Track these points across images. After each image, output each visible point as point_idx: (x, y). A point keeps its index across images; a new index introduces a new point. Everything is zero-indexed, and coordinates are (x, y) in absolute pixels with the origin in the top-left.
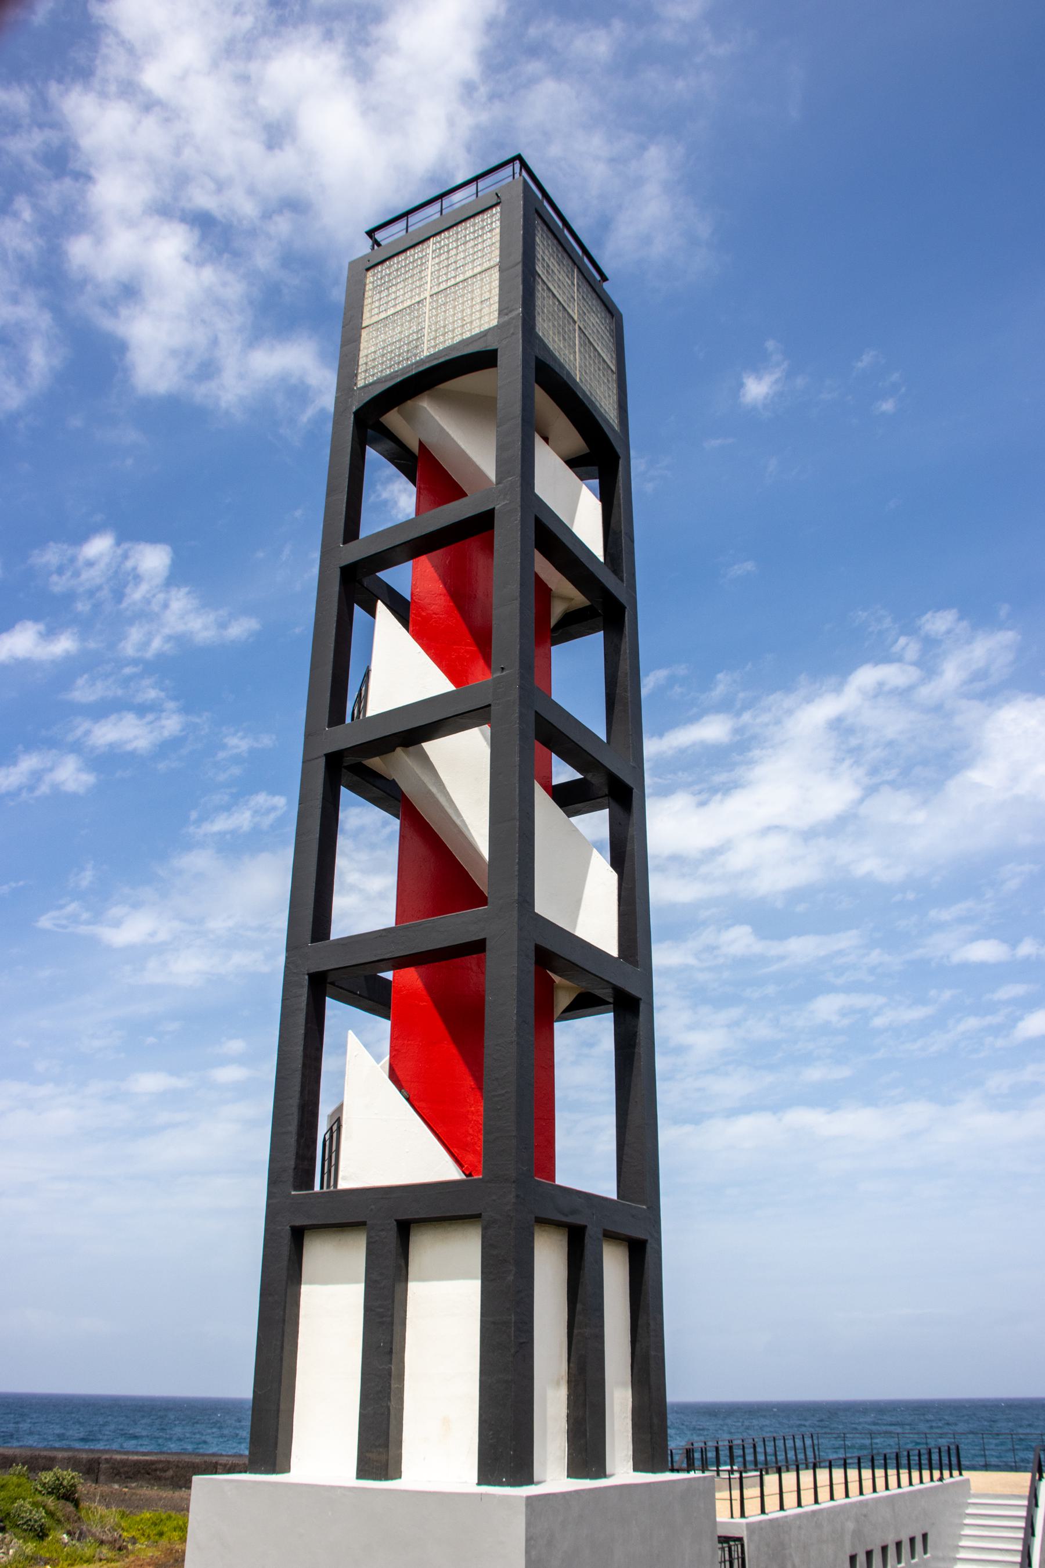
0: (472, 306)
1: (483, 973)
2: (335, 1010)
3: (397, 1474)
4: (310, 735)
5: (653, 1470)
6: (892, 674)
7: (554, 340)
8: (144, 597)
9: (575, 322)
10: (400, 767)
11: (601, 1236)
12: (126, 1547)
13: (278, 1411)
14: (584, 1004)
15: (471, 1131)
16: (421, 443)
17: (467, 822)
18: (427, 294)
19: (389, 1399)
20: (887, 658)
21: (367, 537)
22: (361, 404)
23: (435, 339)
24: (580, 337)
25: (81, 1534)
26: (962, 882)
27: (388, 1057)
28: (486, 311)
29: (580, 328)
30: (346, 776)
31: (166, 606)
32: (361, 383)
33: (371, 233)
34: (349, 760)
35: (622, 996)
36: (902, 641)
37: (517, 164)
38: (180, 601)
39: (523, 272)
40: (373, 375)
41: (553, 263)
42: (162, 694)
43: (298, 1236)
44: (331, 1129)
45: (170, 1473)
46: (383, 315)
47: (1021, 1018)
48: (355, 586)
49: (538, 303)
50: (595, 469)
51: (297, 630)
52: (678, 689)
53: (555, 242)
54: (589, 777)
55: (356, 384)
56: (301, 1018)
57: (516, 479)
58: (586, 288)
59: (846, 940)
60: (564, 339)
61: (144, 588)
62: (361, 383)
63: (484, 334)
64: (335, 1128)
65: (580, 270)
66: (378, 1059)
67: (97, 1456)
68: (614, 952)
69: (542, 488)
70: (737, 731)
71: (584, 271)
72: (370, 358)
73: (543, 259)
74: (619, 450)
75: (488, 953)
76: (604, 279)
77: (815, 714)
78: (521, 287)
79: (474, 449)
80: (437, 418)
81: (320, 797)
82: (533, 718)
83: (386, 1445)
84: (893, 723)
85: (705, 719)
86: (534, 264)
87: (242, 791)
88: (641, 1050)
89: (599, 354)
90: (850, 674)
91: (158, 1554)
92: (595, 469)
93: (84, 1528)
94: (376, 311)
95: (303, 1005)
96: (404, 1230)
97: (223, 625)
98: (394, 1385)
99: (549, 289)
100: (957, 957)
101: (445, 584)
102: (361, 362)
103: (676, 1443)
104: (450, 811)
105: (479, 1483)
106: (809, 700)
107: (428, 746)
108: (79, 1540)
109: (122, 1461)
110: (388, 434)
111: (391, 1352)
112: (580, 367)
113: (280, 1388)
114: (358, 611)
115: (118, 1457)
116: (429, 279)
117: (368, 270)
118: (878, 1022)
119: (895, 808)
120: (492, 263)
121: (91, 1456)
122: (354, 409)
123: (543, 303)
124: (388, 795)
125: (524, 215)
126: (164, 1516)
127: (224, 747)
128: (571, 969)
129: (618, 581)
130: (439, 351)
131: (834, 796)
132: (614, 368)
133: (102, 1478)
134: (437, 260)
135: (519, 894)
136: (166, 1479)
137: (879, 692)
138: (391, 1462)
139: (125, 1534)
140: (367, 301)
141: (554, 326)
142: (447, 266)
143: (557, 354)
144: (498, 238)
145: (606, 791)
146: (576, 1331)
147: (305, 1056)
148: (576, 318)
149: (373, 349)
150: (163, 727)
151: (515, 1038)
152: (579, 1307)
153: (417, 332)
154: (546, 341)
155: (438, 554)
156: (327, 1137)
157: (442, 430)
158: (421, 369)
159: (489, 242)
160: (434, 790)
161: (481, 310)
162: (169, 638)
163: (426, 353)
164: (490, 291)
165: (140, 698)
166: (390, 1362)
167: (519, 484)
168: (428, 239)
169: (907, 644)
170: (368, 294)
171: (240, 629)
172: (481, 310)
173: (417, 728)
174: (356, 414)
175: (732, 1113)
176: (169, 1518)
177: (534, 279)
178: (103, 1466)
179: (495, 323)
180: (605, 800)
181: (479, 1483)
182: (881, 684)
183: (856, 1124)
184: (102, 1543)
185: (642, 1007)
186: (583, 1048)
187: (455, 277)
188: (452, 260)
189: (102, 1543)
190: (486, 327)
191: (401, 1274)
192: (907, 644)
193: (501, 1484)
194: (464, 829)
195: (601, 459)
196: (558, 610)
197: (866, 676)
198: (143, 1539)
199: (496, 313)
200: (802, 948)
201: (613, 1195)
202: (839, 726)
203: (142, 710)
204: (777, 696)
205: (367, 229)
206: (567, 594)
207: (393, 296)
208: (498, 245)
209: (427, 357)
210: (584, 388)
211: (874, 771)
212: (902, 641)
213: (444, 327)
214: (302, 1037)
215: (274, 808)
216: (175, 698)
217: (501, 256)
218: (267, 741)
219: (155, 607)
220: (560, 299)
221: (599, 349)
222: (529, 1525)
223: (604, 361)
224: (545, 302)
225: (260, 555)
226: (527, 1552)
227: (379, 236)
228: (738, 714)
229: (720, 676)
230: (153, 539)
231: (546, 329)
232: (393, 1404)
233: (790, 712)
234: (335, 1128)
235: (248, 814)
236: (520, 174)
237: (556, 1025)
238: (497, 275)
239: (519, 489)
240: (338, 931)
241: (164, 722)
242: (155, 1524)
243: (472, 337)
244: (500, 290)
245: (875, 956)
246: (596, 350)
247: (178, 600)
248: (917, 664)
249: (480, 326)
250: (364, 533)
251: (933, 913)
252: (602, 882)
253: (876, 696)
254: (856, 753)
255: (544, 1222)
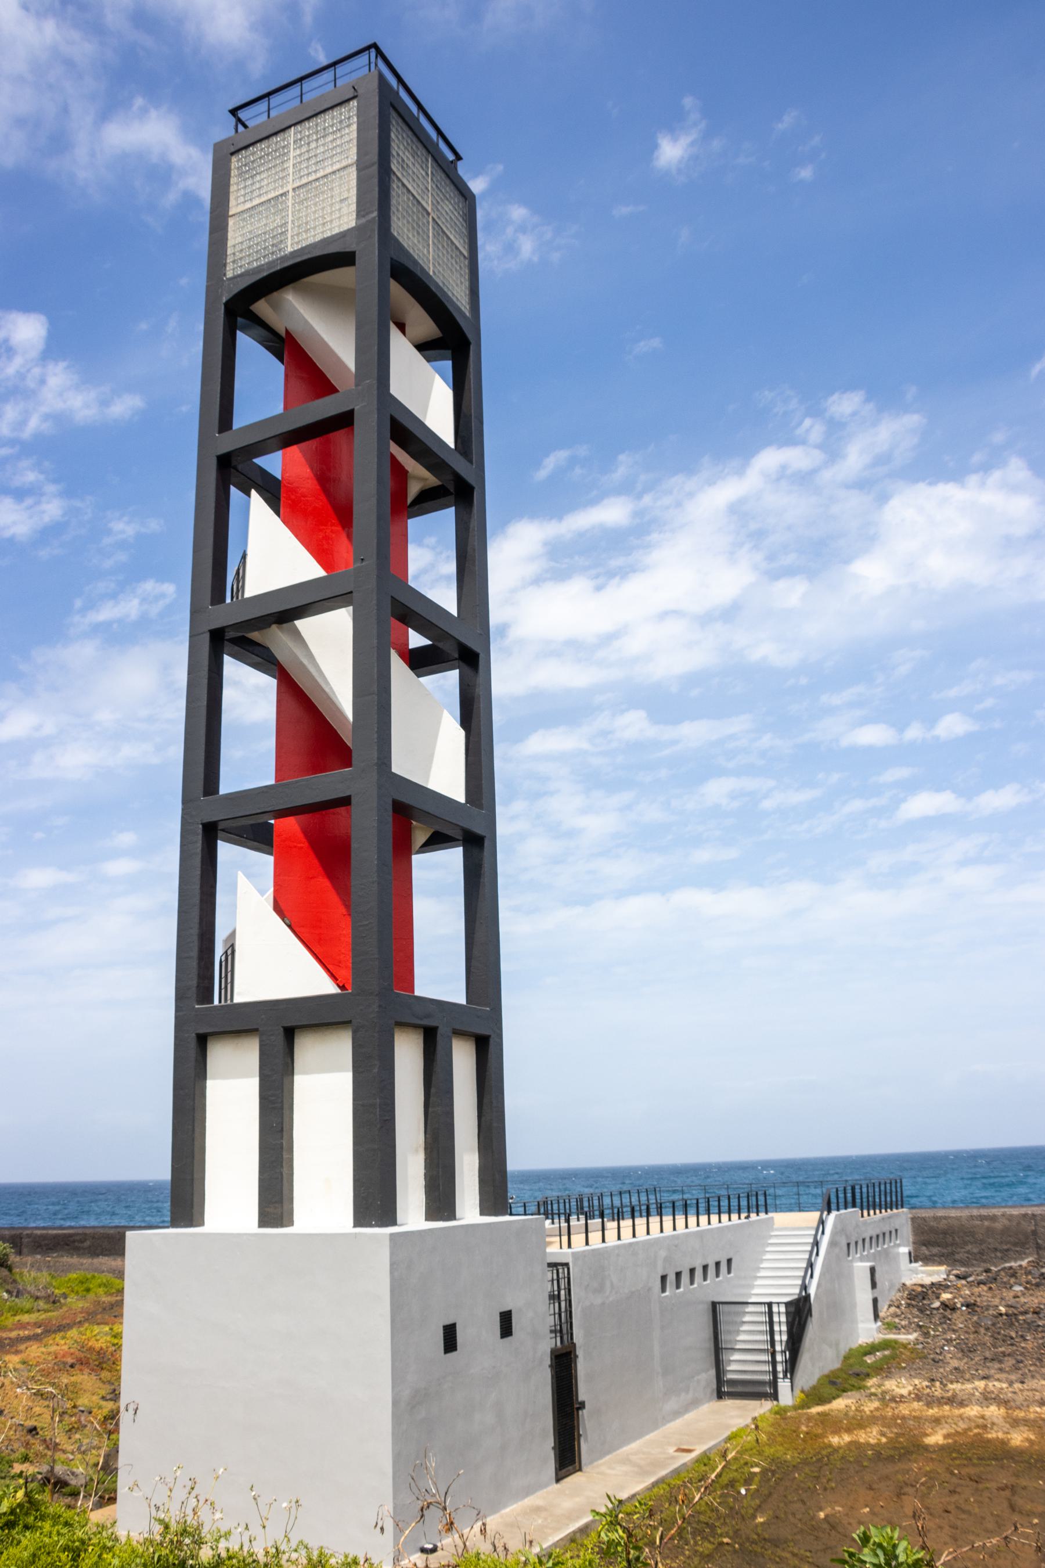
0: (332, 205)
1: (350, 816)
2: (226, 852)
3: (291, 1223)
4: (196, 611)
5: (496, 1214)
6: (796, 457)
7: (408, 238)
8: (18, 372)
9: (428, 214)
10: (277, 639)
11: (450, 1034)
12: (59, 1301)
13: (192, 1180)
14: (437, 841)
15: (343, 951)
16: (287, 331)
17: (335, 689)
18: (290, 187)
19: (282, 1166)
20: (791, 441)
21: (241, 429)
22: (231, 295)
23: (298, 234)
24: (434, 228)
25: (18, 1292)
26: (856, 667)
27: (272, 889)
28: (345, 211)
29: (433, 219)
30: (227, 646)
31: (43, 382)
32: (230, 274)
33: (234, 112)
34: (230, 634)
35: (472, 835)
36: (808, 422)
37: (373, 52)
38: (58, 377)
39: (379, 172)
40: (241, 267)
41: (407, 156)
42: (42, 477)
43: (202, 1041)
44: (226, 952)
45: (87, 1244)
46: (248, 205)
47: (904, 800)
48: (231, 470)
49: (393, 202)
50: (449, 353)
51: (184, 409)
52: (578, 471)
53: (410, 133)
54: (440, 645)
55: (225, 275)
56: (197, 861)
57: (372, 382)
58: (440, 175)
59: (738, 725)
60: (418, 233)
61: (18, 362)
62: (230, 274)
63: (343, 235)
64: (229, 952)
65: (435, 159)
66: (262, 893)
67: (18, 1232)
68: (461, 798)
69: (398, 389)
70: (637, 514)
71: (437, 157)
72: (238, 248)
73: (398, 155)
74: (470, 336)
75: (353, 807)
76: (459, 158)
77: (716, 496)
78: (377, 189)
79: (334, 339)
80: (302, 311)
81: (206, 669)
82: (389, 602)
83: (281, 1202)
84: (793, 507)
85: (605, 501)
86: (389, 162)
87: (131, 576)
88: (486, 879)
89: (452, 242)
90: (753, 456)
91: (87, 1305)
92: (449, 353)
93: (21, 1287)
94: (242, 199)
95: (199, 850)
96: (290, 1034)
97: (105, 403)
98: (285, 1156)
99: (404, 185)
100: (845, 742)
101: (312, 469)
102: (229, 251)
103: (513, 1192)
104: (320, 680)
105: (355, 1226)
106: (711, 482)
107: (301, 624)
108: (17, 1296)
109: (42, 1236)
110: (258, 321)
111: (282, 1130)
112: (434, 259)
113: (193, 1162)
114: (234, 492)
115: (38, 1232)
116: (291, 170)
117: (232, 154)
118: (767, 804)
119: (792, 593)
120: (350, 161)
121: (13, 1232)
122: (224, 300)
123: (398, 200)
124: (264, 660)
125: (380, 112)
126: (89, 1276)
127: (109, 532)
128: (427, 817)
129: (468, 464)
130: (302, 248)
131: (731, 580)
132: (466, 254)
133: (25, 1250)
134: (298, 152)
135: (378, 758)
136: (84, 1249)
137: (782, 475)
138: (285, 1214)
139: (57, 1291)
140: (233, 188)
141: (408, 222)
142: (308, 159)
143: (411, 251)
144: (355, 135)
145: (457, 656)
146: (430, 1110)
147: (202, 893)
148: (429, 210)
149: (240, 239)
150: (44, 512)
151: (375, 879)
152: (433, 1090)
153: (281, 226)
154: (401, 240)
155: (304, 445)
156: (223, 958)
157: (306, 322)
158: (286, 264)
159: (346, 138)
160: (305, 662)
161: (340, 209)
162: (47, 417)
163: (290, 249)
164: (348, 191)
165: (18, 481)
166: (282, 1138)
167: (375, 387)
168: (290, 127)
169: (811, 427)
170: (233, 180)
171: (125, 406)
172: (340, 209)
173: (290, 608)
174: (227, 305)
175: (621, 894)
176: (94, 1277)
177: (390, 178)
178: (25, 1240)
179: (353, 224)
180: (456, 662)
181: (355, 1226)
182: (784, 467)
183: (744, 904)
184: (37, 1298)
185: (487, 843)
186: (436, 877)
187: (315, 172)
188: (312, 154)
189: (37, 1298)
190: (345, 227)
191: (288, 1069)
192: (811, 427)
193: (371, 1226)
194: (332, 696)
195: (453, 343)
196: (413, 490)
197: (770, 459)
198: (73, 1295)
199: (354, 214)
200: (694, 733)
201: (462, 1000)
202: (737, 510)
203: (19, 494)
204: (678, 479)
205: (231, 108)
206: (420, 477)
207: (258, 185)
208: (355, 142)
209: (291, 253)
210: (438, 281)
211: (771, 558)
212: (808, 422)
213: (307, 223)
214: (199, 877)
215: (163, 596)
216: (55, 481)
217: (358, 153)
218: (154, 525)
219: (31, 383)
220: (415, 193)
221: (452, 237)
222: (392, 1254)
223: (457, 248)
224: (400, 200)
225: (144, 326)
226: (391, 1273)
227: (243, 115)
228: (639, 497)
229: (622, 457)
230: (27, 307)
231: (402, 230)
232: (285, 1171)
233: (691, 495)
234: (229, 952)
235: (136, 602)
236: (376, 65)
237: (415, 858)
238: (355, 173)
239: (375, 392)
240: (226, 787)
241: (45, 507)
242: (82, 1282)
243: (333, 236)
244: (358, 190)
245: (766, 741)
246: (448, 238)
247: (55, 375)
248: (819, 447)
249: (339, 226)
250: (238, 423)
251: (824, 698)
252: (451, 738)
253: (778, 479)
254: (759, 535)
255: (402, 1025)
